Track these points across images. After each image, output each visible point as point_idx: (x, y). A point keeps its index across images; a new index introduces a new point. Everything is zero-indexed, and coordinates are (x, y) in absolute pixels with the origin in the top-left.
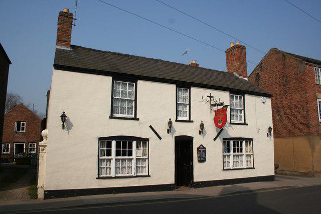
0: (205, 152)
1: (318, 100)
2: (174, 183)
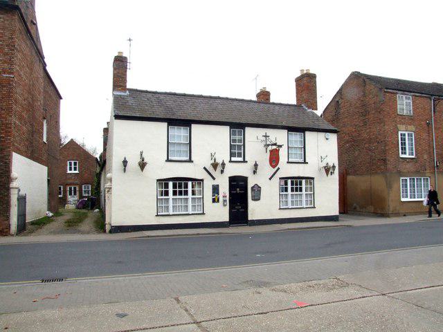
0: (260, 191)
1: (400, 133)
2: (228, 220)
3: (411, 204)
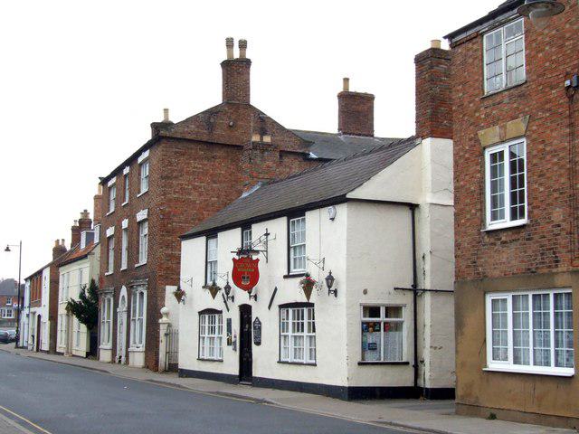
3: (511, 383)
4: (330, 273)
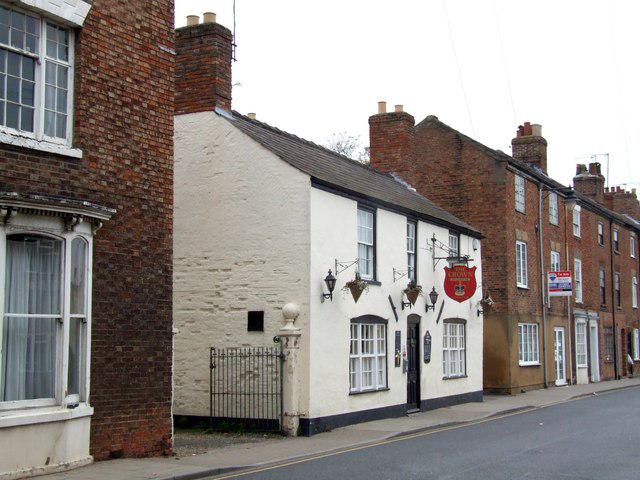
4: (434, 289)
